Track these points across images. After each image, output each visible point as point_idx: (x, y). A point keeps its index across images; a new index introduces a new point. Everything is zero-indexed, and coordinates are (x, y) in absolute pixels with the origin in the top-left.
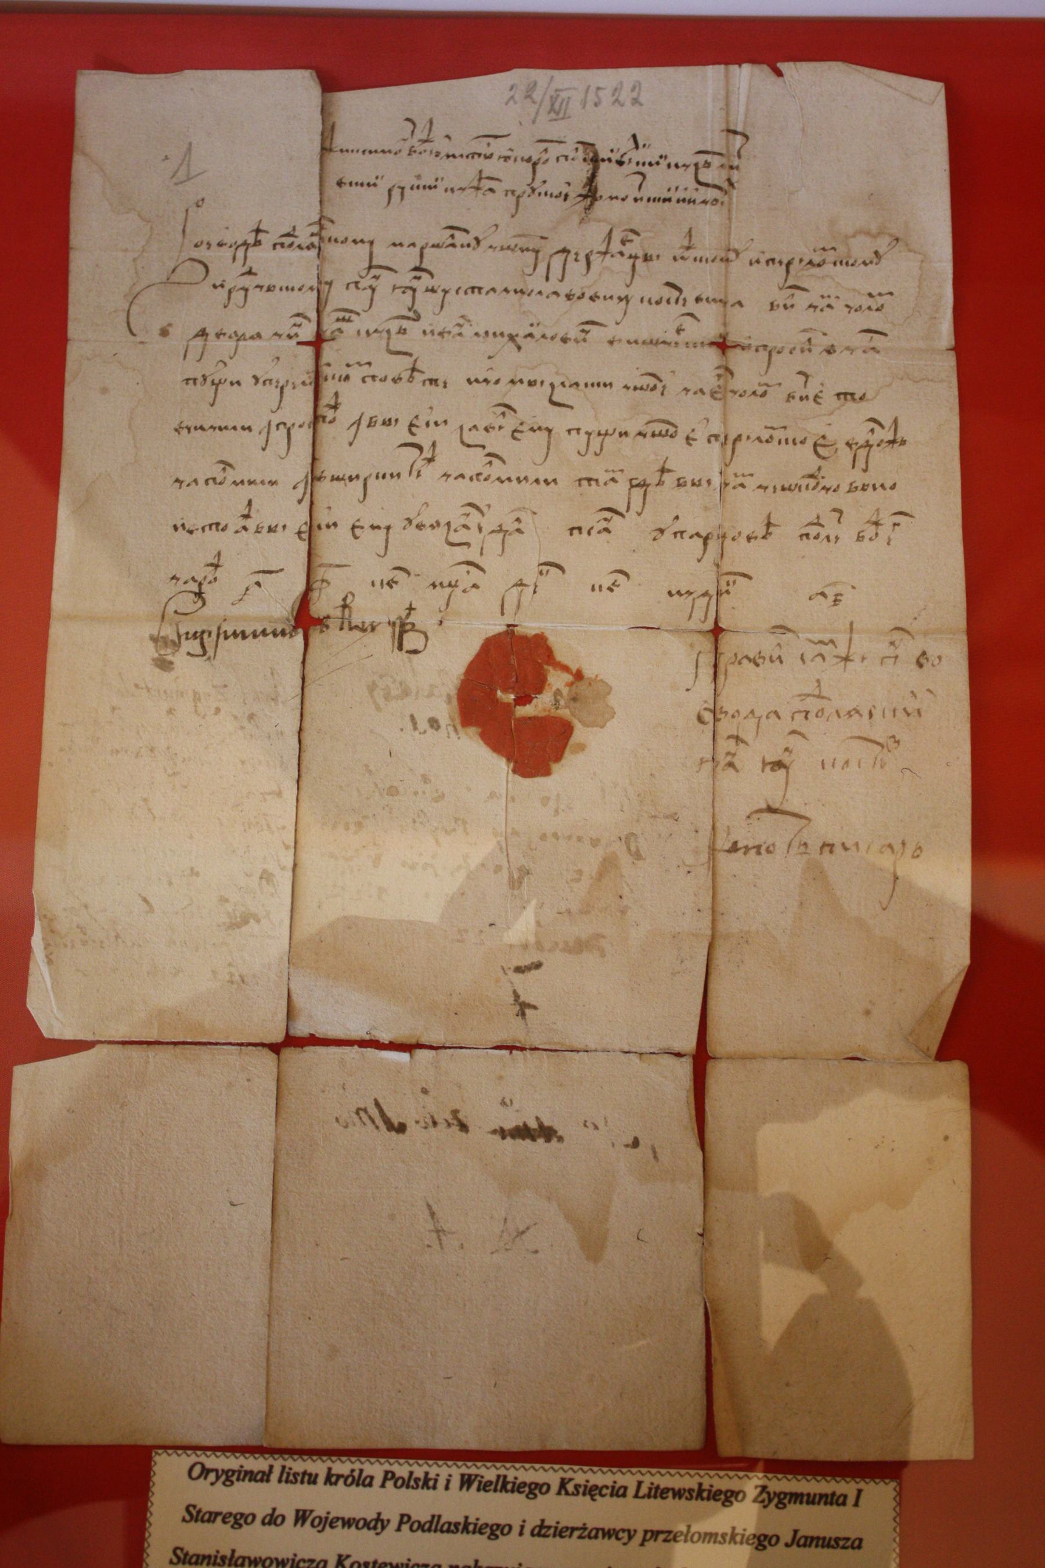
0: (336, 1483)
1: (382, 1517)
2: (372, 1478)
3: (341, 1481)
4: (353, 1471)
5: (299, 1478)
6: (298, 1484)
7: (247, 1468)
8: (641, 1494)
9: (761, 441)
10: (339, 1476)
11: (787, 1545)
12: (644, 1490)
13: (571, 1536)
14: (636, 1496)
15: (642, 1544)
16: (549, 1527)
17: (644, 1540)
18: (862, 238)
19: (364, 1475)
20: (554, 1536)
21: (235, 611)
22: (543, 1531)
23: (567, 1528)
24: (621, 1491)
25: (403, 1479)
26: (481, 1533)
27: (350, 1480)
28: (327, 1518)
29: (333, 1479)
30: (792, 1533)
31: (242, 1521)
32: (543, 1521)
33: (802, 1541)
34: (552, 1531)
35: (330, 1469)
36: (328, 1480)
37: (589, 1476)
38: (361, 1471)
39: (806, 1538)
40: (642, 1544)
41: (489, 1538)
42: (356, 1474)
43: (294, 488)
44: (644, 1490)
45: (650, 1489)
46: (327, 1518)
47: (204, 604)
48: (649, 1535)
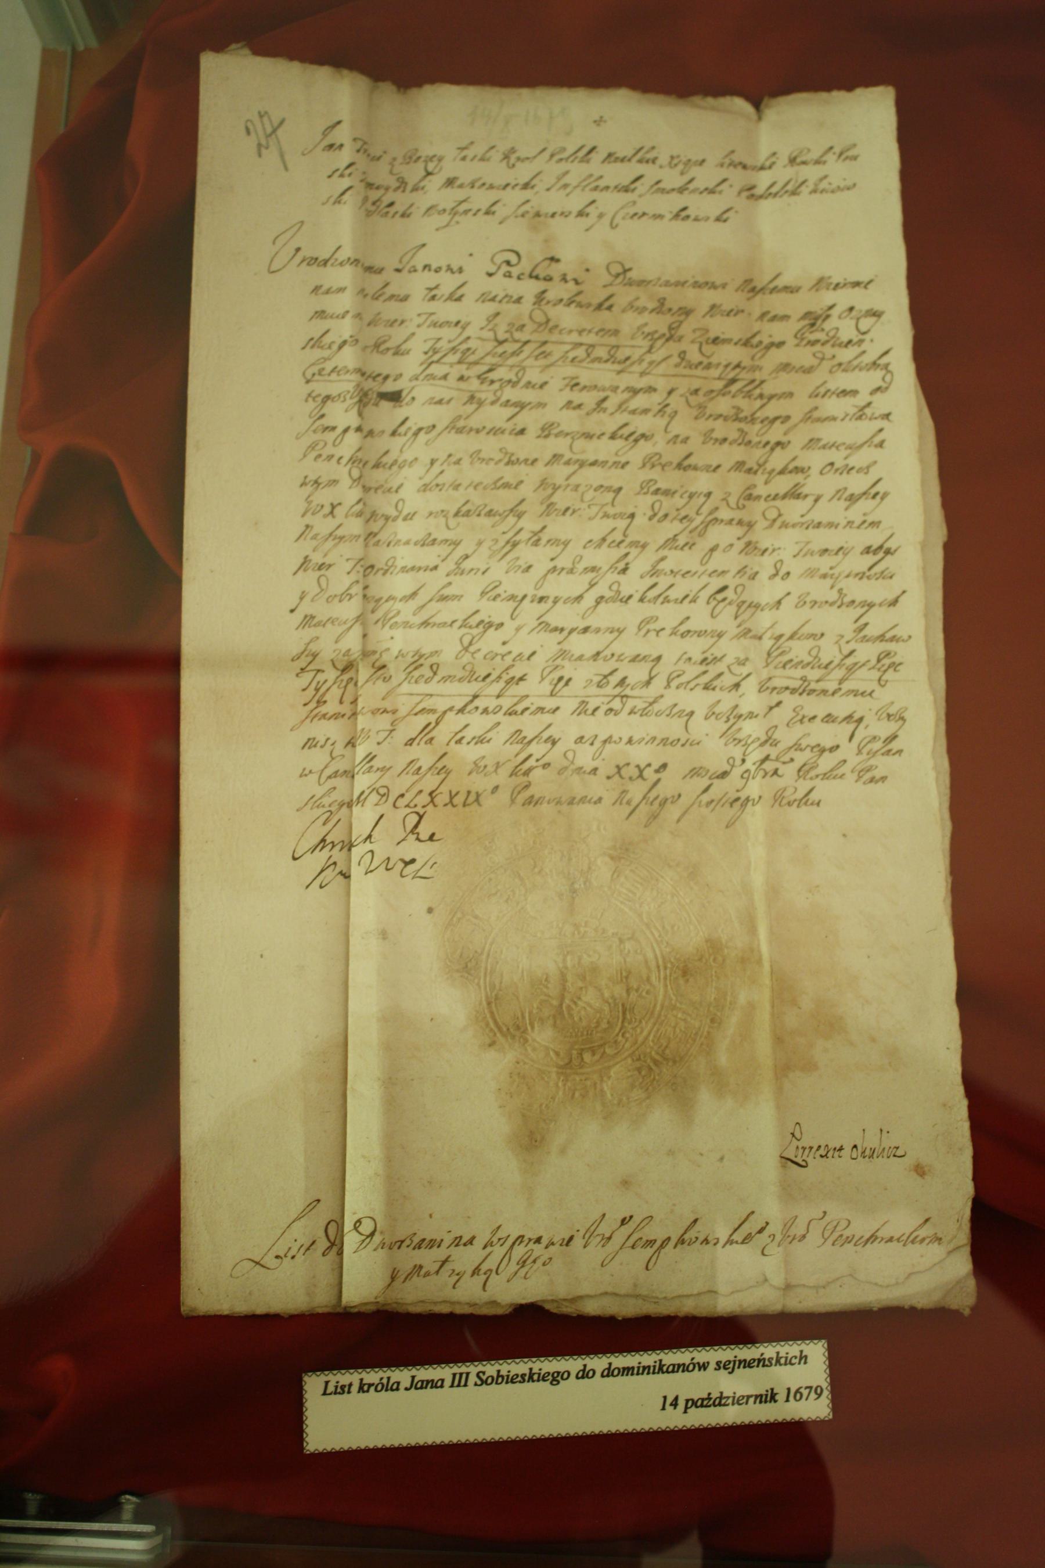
0: (368, 1391)
1: (501, 1373)
2: (443, 1380)
3: (372, 1389)
4: (381, 1379)
5: (346, 1389)
6: (345, 1395)
7: (645, 1363)
8: (328, 1392)
9: (453, 272)
10: (370, 1385)
11: (406, 1389)
12: (331, 1388)
13: (747, 1403)
14: (452, 1386)
15: (685, 1412)
16: (728, 1398)
17: (686, 1408)
18: (704, 350)
19: (392, 1381)
20: (733, 1404)
21: (676, 668)
22: (723, 1401)
23: (743, 1397)
24: (439, 1384)
25: (493, 1377)
26: (544, 1380)
27: (379, 1387)
28: (508, 1376)
29: (366, 1388)
30: (410, 1379)
31: (559, 1378)
32: (722, 1393)
33: (419, 1385)
34: (730, 1401)
35: (362, 1380)
36: (361, 1389)
37: (695, 1354)
38: (389, 1378)
39: (423, 1381)
40: (685, 1412)
41: (551, 1383)
42: (385, 1381)
43: (425, 341)
44: (331, 1388)
45: (336, 1387)
46: (508, 1376)
47: (304, 374)
48: (690, 1403)
